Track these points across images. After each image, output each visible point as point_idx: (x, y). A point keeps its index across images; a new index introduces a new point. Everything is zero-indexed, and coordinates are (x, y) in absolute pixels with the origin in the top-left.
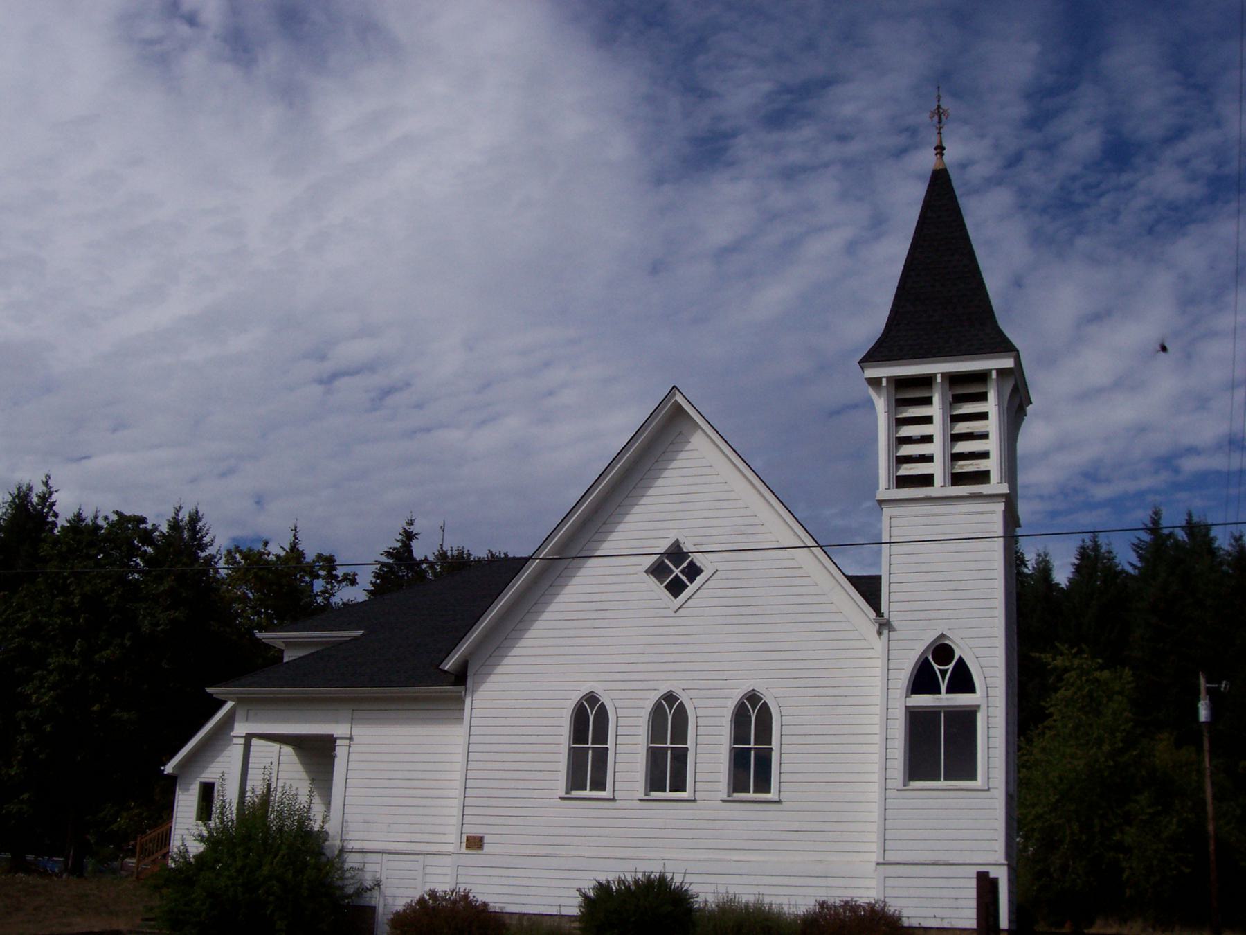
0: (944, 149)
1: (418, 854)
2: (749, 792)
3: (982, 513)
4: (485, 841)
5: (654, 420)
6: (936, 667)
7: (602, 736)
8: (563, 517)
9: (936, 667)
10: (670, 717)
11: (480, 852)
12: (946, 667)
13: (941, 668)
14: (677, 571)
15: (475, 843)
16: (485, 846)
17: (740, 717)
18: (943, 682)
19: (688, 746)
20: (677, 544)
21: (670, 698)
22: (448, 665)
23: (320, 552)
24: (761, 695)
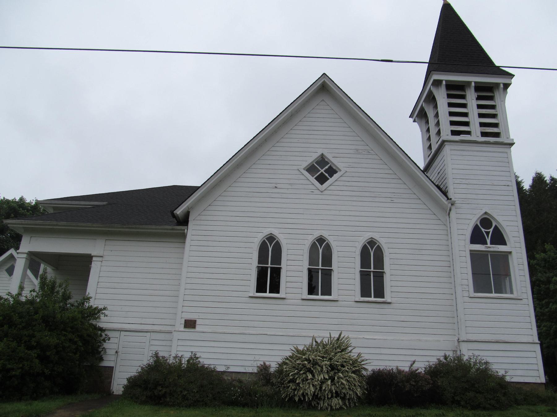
1: (147, 332)
4: (198, 323)
6: (483, 230)
8: (337, 84)
9: (483, 230)
10: (321, 251)
11: (193, 330)
14: (322, 171)
15: (190, 324)
16: (197, 326)
17: (365, 253)
18: (488, 238)
20: (322, 156)
21: (321, 240)
22: (179, 211)
24: (375, 241)
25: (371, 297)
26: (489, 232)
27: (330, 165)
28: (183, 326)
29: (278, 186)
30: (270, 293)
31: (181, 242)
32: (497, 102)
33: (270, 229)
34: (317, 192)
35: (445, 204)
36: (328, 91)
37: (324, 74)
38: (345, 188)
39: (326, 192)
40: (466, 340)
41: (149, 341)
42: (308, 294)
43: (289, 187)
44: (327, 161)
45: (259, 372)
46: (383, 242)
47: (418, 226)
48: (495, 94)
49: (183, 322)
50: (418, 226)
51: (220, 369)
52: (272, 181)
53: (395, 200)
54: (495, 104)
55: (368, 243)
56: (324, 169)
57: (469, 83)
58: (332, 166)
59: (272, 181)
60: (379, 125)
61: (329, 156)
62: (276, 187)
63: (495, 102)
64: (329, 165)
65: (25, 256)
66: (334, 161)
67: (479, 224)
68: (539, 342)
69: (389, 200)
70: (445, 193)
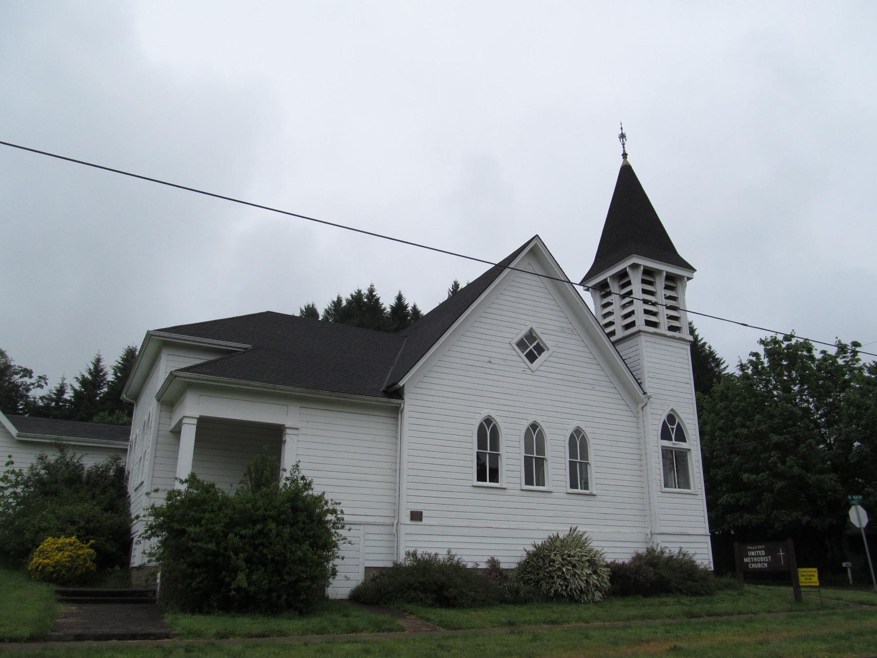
0: (627, 155)
2: (486, 481)
3: (669, 346)
4: (424, 515)
5: (551, 259)
6: (669, 426)
7: (495, 445)
9: (669, 426)
11: (419, 523)
12: (673, 427)
13: (672, 427)
15: (416, 516)
19: (500, 453)
20: (531, 331)
23: (852, 341)
24: (581, 430)
25: (578, 488)
26: (674, 428)
27: (538, 342)
28: (409, 518)
29: (493, 360)
30: (490, 482)
31: (383, 416)
32: (679, 294)
33: (488, 410)
34: (528, 371)
35: (641, 397)
36: (534, 254)
37: (537, 235)
38: (553, 370)
39: (537, 373)
40: (660, 533)
41: (363, 536)
42: (478, 481)
43: (502, 363)
44: (535, 337)
45: (518, 569)
46: (588, 431)
47: (615, 417)
48: (656, 279)
49: (409, 514)
50: (615, 417)
51: (470, 566)
52: (486, 354)
53: (597, 388)
54: (677, 296)
55: (485, 421)
56: (533, 345)
57: (660, 272)
58: (540, 343)
59: (486, 354)
60: (586, 302)
61: (538, 331)
62: (490, 362)
63: (677, 293)
64: (536, 342)
65: (195, 421)
66: (543, 338)
67: (666, 420)
68: (710, 534)
69: (590, 387)
70: (640, 384)
